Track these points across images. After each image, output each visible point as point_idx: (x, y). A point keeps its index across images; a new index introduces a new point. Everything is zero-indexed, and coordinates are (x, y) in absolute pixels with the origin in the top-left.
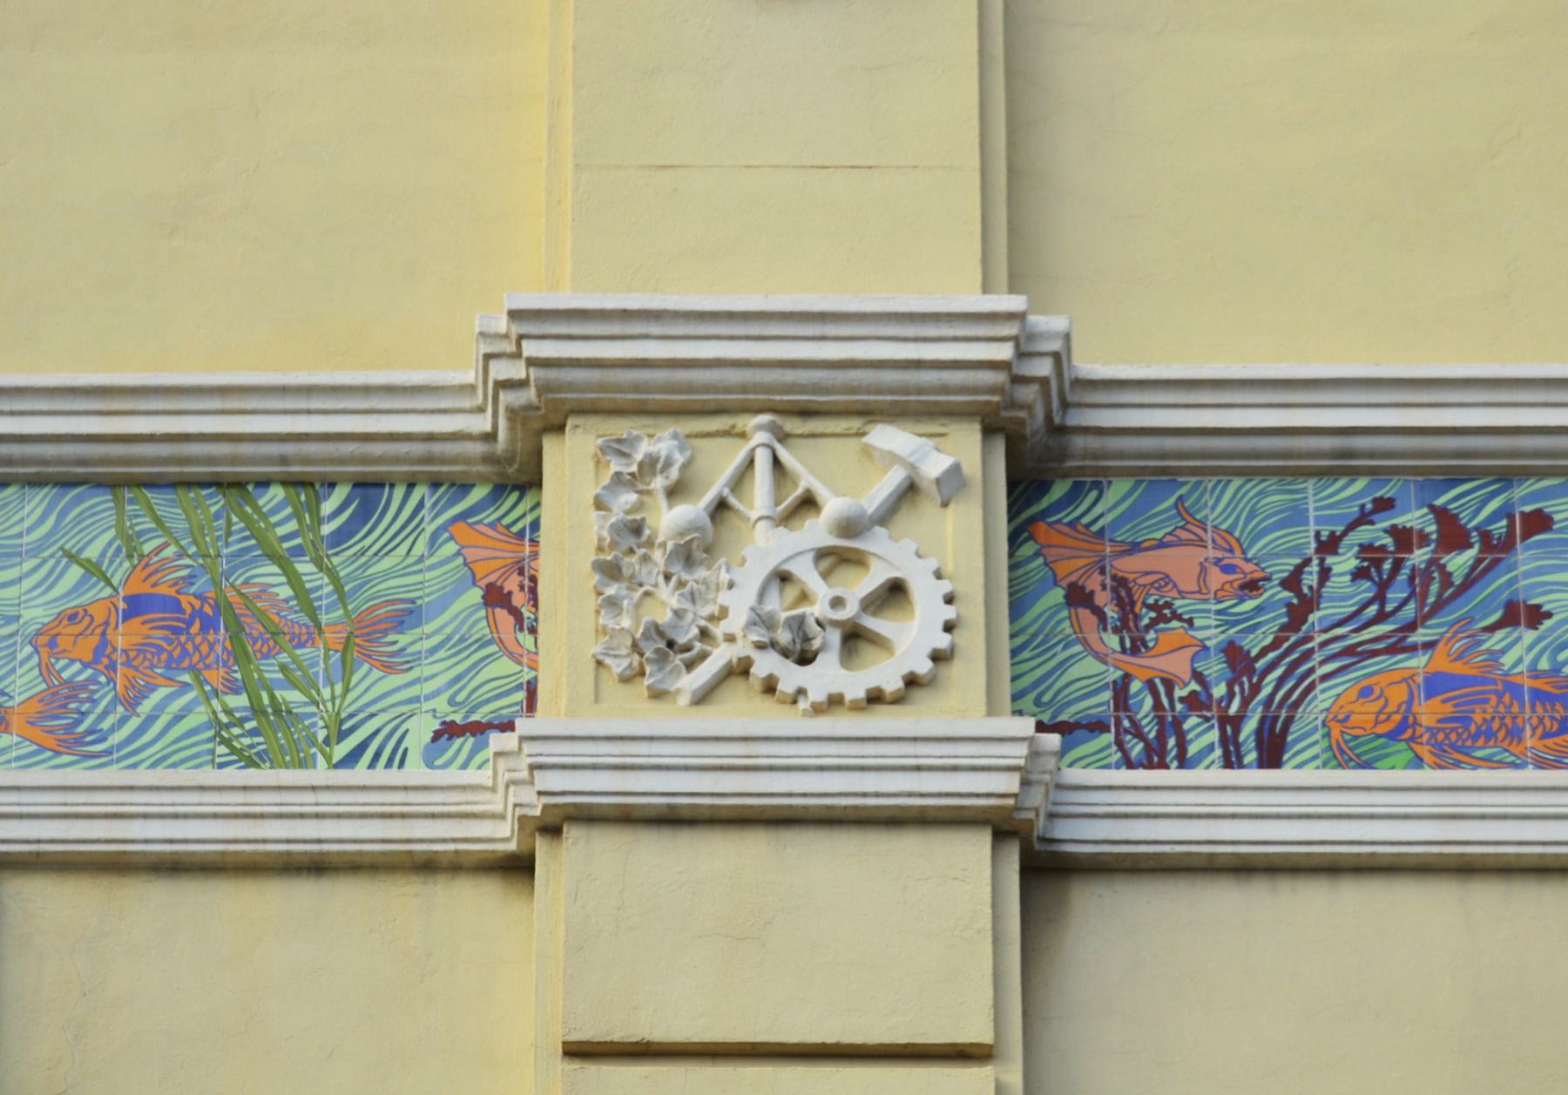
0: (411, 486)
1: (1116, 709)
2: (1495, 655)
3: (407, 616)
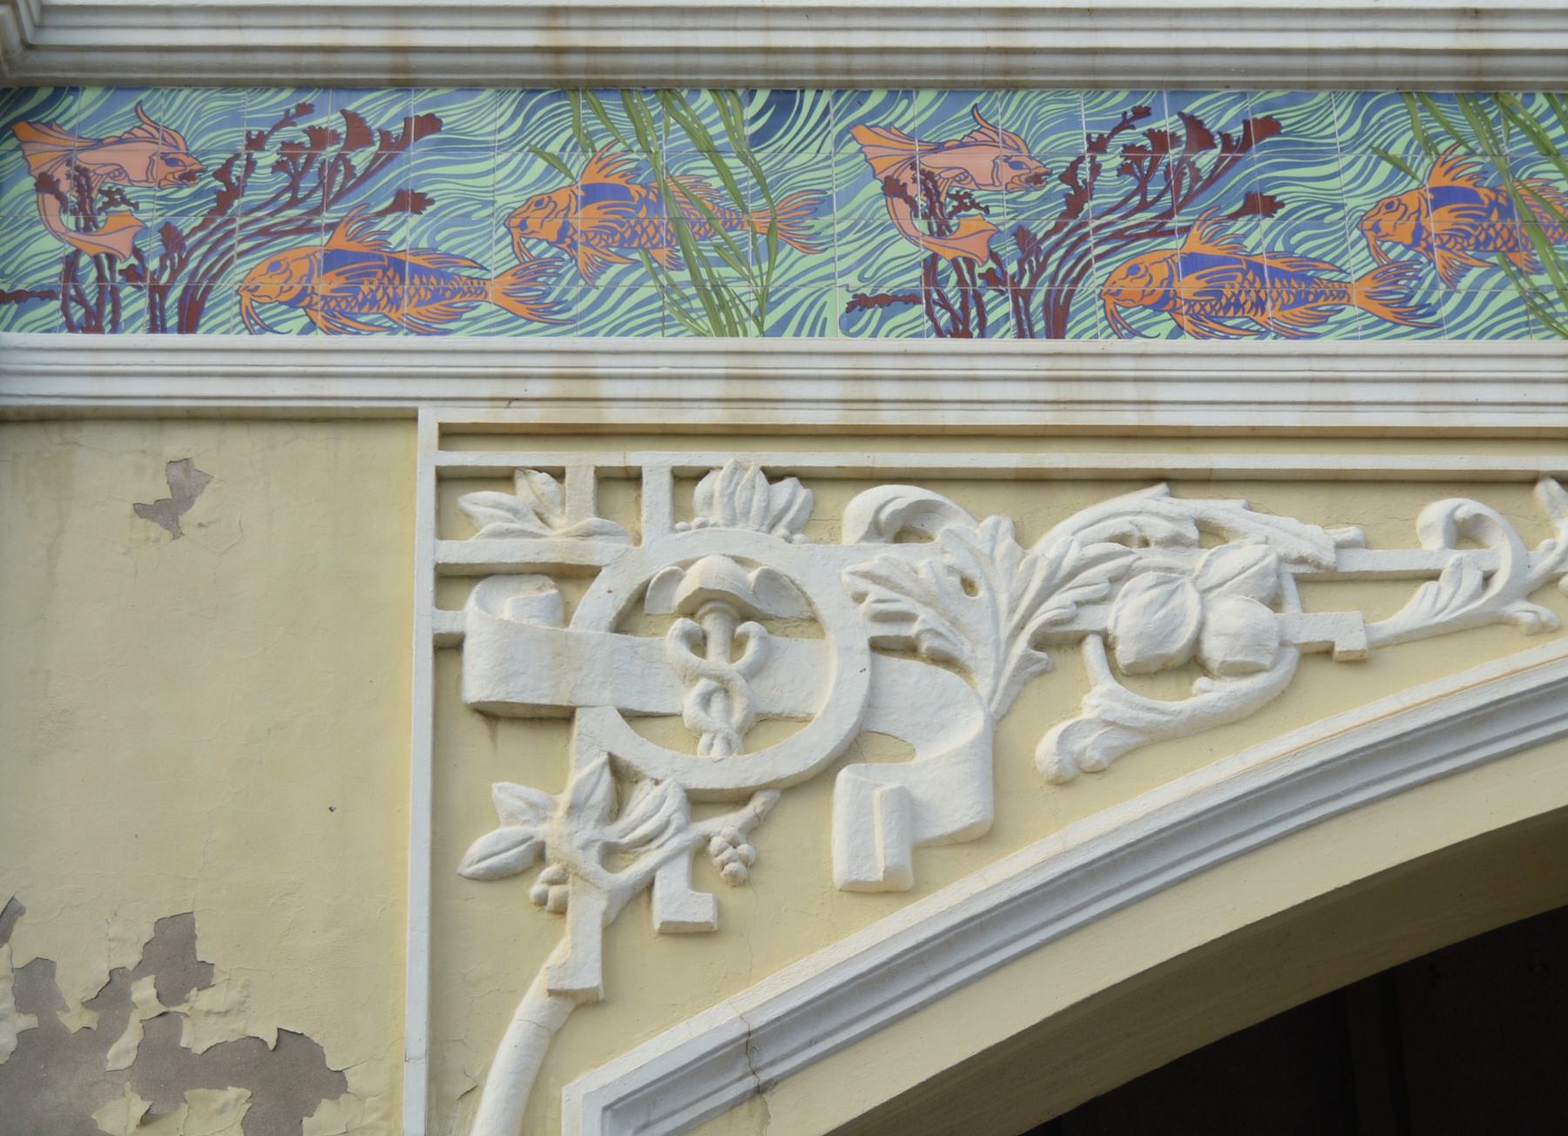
0: (819, 92)
1: (66, 280)
2: (1239, 239)
3: (820, 204)
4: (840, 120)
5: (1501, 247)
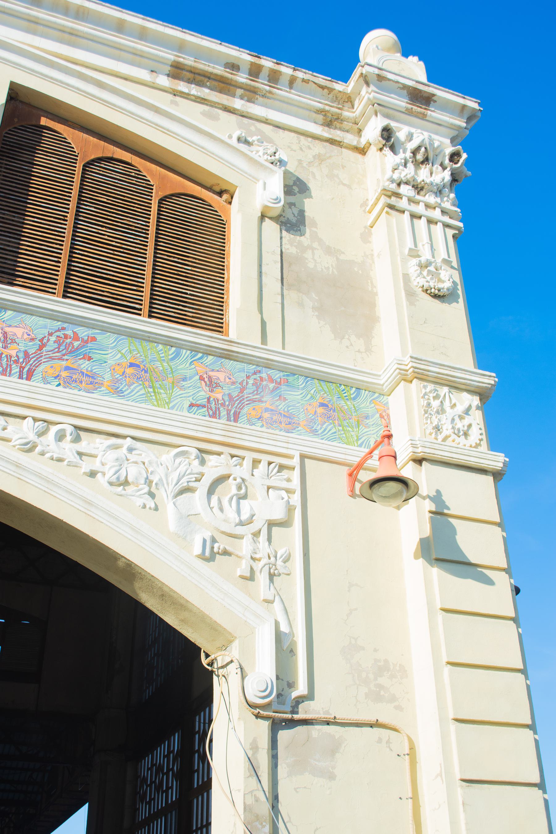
2: (80, 365)
4: (191, 359)
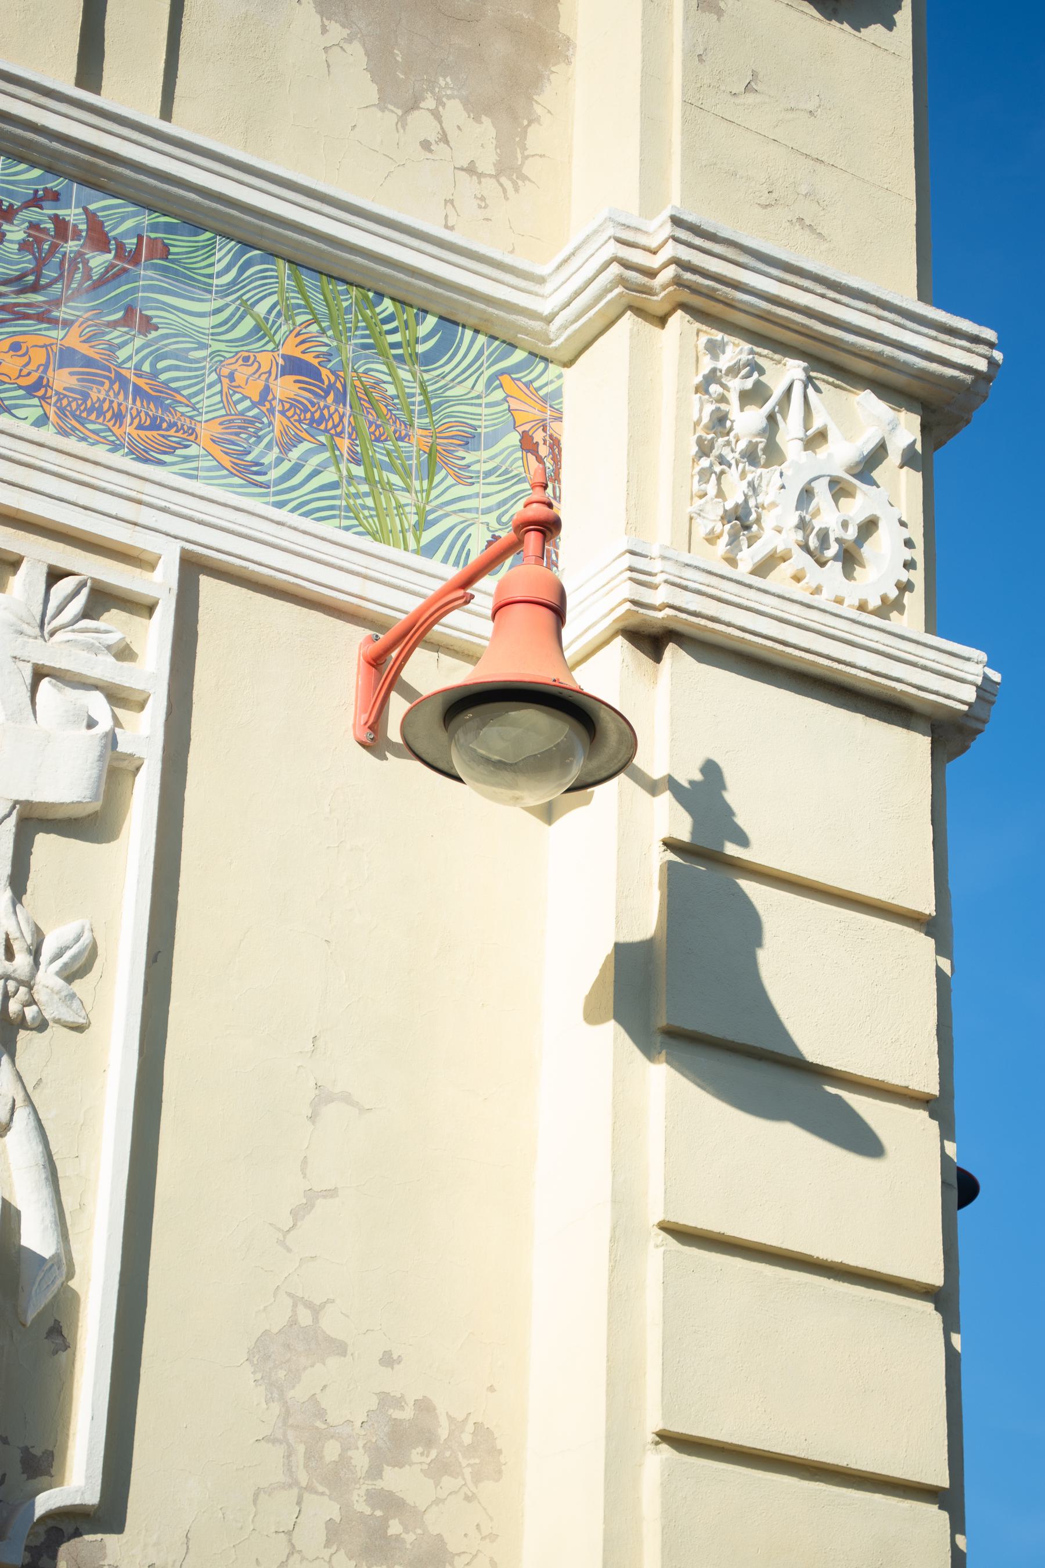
3: (469, 440)
5: (331, 429)
